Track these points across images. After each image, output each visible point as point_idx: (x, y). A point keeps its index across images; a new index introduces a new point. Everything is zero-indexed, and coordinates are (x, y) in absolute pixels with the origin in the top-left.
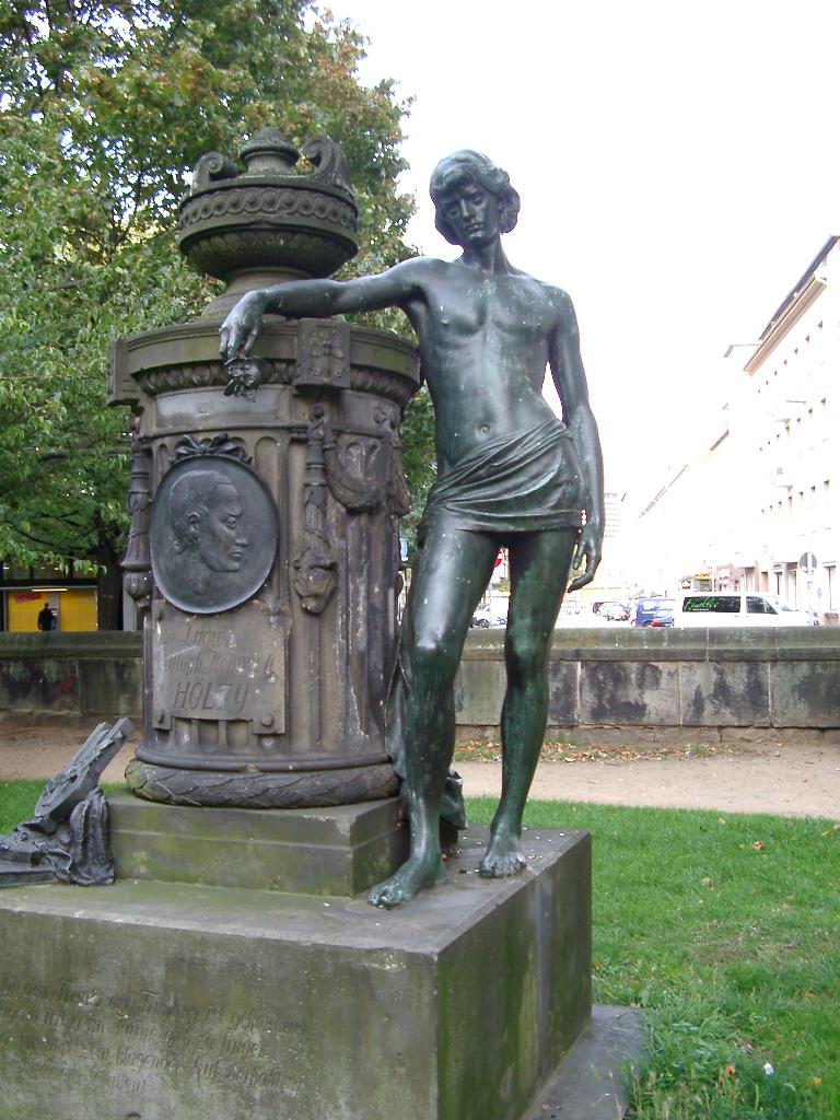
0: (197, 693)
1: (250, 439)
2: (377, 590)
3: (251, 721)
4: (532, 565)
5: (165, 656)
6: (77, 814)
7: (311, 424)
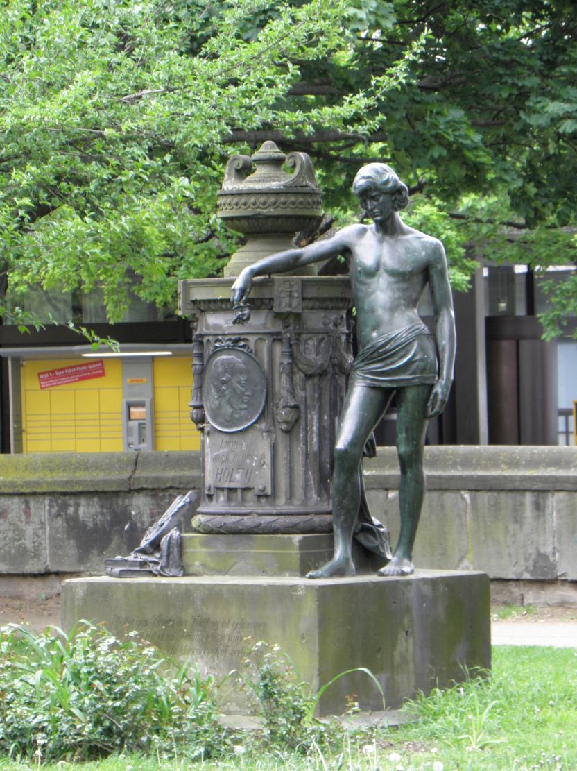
0: (226, 474)
1: (252, 339)
2: (326, 418)
4: (403, 404)
6: (164, 541)
7: (283, 331)
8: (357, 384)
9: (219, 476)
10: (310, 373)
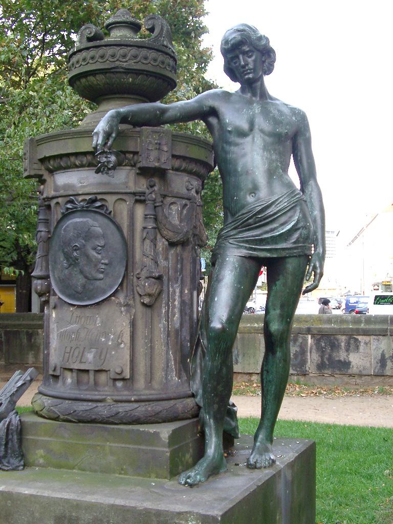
0: (76, 354)
1: (111, 199)
2: (186, 292)
3: (109, 370)
4: (281, 277)
5: (58, 330)
7: (147, 191)
8: (228, 253)
9: (67, 355)
10: (175, 240)
